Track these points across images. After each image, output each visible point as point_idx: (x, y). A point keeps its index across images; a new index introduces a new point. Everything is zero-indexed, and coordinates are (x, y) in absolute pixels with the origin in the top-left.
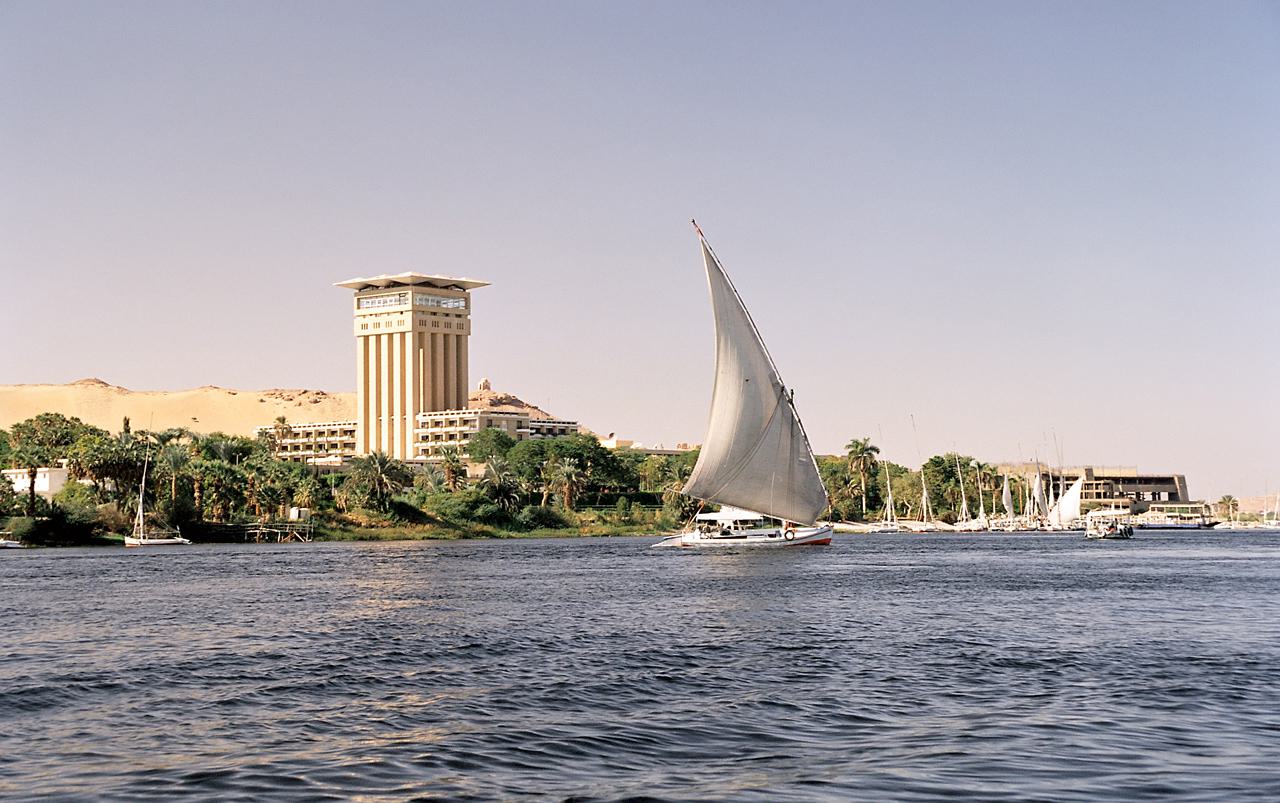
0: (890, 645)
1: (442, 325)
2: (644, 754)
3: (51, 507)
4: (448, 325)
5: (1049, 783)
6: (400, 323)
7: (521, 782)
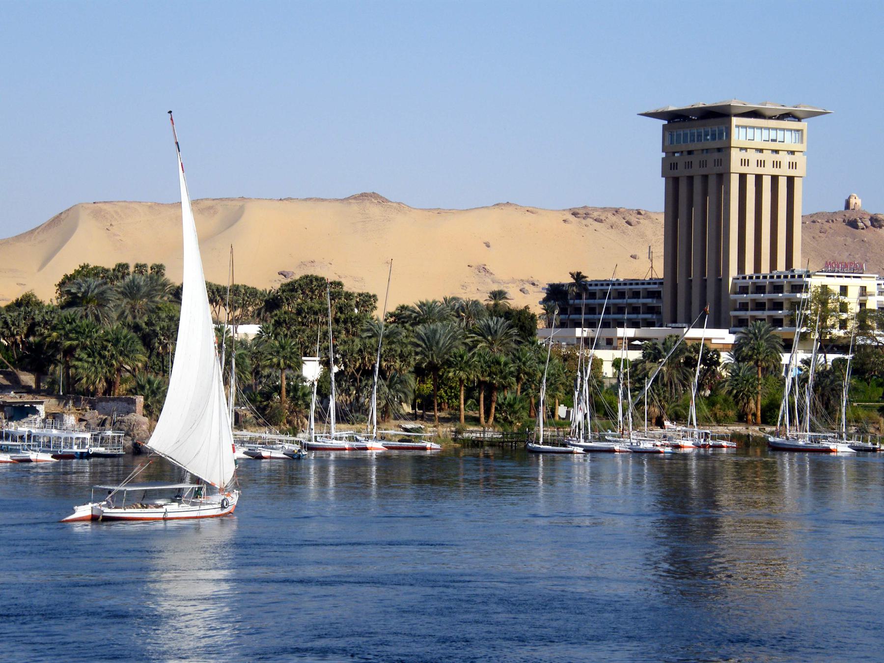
1: (769, 164)
4: (703, 164)
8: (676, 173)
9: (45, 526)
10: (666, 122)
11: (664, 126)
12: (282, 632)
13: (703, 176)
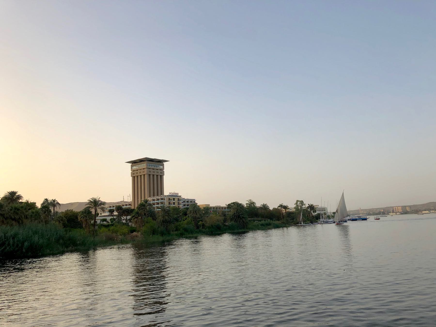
0: (39, 261)
1: (156, 172)
2: (86, 285)
3: (180, 210)
4: (154, 172)
5: (317, 315)
6: (144, 172)
7: (348, 314)
8: (134, 175)
9: (113, 320)
10: (132, 164)
11: (131, 165)
12: (29, 228)
13: (137, 176)
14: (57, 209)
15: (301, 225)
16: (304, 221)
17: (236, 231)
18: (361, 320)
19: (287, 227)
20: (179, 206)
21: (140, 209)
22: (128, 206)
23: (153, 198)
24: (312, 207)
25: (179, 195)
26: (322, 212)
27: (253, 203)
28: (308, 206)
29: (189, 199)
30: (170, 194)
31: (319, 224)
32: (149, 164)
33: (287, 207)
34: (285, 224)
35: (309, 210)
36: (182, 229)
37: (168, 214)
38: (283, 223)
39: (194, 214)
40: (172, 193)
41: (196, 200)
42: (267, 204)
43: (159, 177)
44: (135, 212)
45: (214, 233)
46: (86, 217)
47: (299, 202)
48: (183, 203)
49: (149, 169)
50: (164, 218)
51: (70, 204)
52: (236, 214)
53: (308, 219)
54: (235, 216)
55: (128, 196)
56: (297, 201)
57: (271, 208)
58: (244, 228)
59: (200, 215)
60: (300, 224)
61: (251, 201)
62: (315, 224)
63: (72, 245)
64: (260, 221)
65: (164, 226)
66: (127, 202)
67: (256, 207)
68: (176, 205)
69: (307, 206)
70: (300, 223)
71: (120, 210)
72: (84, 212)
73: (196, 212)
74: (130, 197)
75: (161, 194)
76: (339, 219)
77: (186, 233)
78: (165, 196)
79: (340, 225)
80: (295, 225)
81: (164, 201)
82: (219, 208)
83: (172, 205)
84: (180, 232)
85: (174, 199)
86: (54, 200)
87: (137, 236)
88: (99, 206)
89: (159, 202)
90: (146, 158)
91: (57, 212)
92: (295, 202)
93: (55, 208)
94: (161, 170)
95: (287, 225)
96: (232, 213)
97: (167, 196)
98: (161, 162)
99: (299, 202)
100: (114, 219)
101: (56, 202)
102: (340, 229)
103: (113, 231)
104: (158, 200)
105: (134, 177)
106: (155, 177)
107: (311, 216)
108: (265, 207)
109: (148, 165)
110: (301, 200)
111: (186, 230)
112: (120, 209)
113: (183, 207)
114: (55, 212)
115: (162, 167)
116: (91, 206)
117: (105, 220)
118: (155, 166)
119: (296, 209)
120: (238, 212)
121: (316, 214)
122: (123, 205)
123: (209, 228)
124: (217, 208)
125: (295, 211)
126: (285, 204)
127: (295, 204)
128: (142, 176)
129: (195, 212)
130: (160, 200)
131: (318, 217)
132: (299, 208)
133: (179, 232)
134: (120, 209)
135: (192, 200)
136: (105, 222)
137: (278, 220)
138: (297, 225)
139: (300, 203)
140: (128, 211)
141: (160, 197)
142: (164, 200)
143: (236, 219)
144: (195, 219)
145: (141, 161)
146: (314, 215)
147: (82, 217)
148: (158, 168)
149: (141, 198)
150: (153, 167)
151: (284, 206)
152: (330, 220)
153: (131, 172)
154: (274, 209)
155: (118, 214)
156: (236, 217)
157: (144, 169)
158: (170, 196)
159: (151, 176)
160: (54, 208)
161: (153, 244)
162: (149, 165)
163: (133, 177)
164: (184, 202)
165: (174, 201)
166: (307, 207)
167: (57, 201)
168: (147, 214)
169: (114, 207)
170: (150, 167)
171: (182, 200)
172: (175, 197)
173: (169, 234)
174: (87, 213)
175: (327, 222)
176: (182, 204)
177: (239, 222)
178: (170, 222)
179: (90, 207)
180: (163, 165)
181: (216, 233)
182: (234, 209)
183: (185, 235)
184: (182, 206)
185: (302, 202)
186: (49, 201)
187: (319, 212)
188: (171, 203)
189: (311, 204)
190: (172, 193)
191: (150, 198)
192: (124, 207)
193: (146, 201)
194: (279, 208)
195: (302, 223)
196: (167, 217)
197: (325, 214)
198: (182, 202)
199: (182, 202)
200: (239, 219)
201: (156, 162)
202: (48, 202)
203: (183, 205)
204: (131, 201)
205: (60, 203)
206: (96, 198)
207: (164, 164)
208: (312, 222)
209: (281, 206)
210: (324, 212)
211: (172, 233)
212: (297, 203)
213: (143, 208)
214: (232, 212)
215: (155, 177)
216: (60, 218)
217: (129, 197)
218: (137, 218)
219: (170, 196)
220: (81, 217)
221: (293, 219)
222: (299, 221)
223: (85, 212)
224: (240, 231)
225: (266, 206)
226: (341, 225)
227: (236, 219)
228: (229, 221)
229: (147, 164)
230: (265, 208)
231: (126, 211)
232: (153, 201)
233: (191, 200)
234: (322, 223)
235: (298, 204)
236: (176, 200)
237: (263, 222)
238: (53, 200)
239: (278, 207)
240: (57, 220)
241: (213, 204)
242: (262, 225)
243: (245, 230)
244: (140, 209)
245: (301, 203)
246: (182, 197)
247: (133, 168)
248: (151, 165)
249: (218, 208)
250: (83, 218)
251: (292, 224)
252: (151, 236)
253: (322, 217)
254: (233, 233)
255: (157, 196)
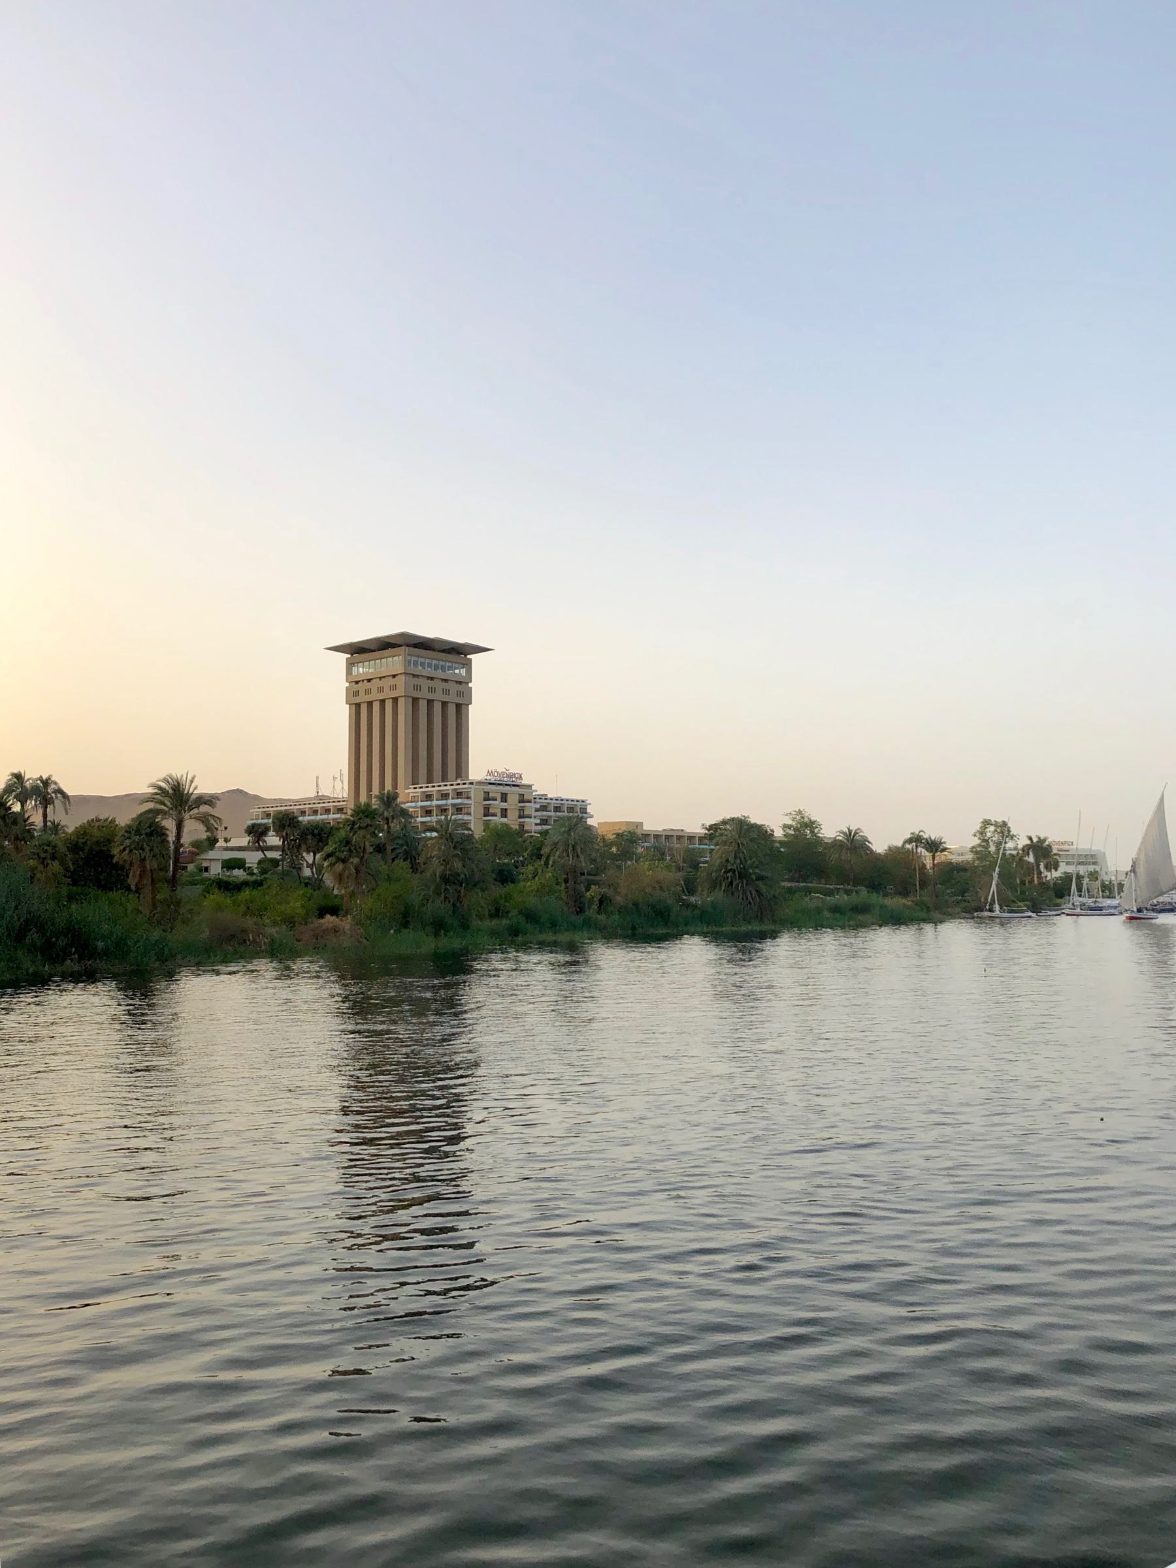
6: (393, 688)
8: (358, 700)
10: (349, 656)
14: (56, 814)
15: (991, 917)
16: (1007, 903)
17: (727, 929)
18: (23, 1405)
19: (937, 922)
20: (522, 825)
21: (357, 826)
22: (331, 816)
23: (427, 787)
24: (1041, 849)
25: (524, 782)
26: (1082, 870)
27: (811, 825)
28: (1029, 842)
29: (562, 800)
30: (489, 777)
31: (1064, 913)
32: (414, 658)
33: (941, 843)
34: (928, 909)
35: (1031, 859)
36: (514, 912)
37: (464, 851)
38: (921, 905)
39: (568, 856)
40: (496, 774)
41: (590, 804)
42: (862, 832)
43: (452, 710)
44: (337, 840)
45: (640, 931)
46: (142, 849)
47: (992, 828)
48: (539, 813)
49: (414, 676)
50: (448, 867)
51: (131, 797)
52: (733, 865)
53: (1023, 892)
54: (731, 870)
55: (334, 778)
56: (986, 823)
57: (879, 846)
58: (761, 920)
59: (593, 861)
60: (987, 914)
61: (803, 818)
62: (1050, 913)
63: (75, 953)
64: (830, 893)
65: (446, 898)
66: (330, 798)
67: (821, 839)
68: (512, 821)
69: (1023, 842)
70: (987, 907)
71: (288, 830)
72: (135, 829)
73: (573, 847)
74: (342, 782)
75: (458, 776)
76: (1139, 900)
77: (529, 926)
78: (471, 783)
79: (1143, 921)
80: (967, 915)
81: (466, 801)
82: (679, 838)
83: (498, 819)
84: (508, 922)
85: (504, 798)
86: (47, 780)
87: (335, 931)
88: (190, 809)
89: (446, 805)
90: (403, 635)
91: (56, 827)
92: (978, 827)
93: (50, 809)
94: (460, 683)
95: (936, 915)
96: (718, 861)
97: (480, 783)
98: (459, 652)
99: (992, 828)
100: (275, 862)
101: (53, 786)
102: (1143, 939)
103: (248, 908)
104: (445, 796)
105: (358, 706)
106: (437, 708)
107: (1036, 882)
108: (854, 844)
109: (410, 662)
110: (1000, 820)
111: (531, 917)
112: (289, 825)
113: (539, 828)
114: (49, 824)
115: (463, 672)
116: (163, 807)
117: (239, 864)
118: (436, 667)
119: (977, 853)
120: (741, 855)
121: (1056, 874)
122: (303, 813)
123: (621, 910)
124: (668, 837)
125: (974, 861)
126: (931, 834)
127: (975, 836)
128: (374, 703)
129: (570, 849)
130: (452, 799)
131: (1061, 890)
132: (992, 849)
133: (505, 921)
134: (289, 825)
135: (549, 801)
136: (236, 872)
137: (905, 893)
138: (975, 914)
139: (996, 831)
140: (319, 834)
141: (453, 787)
142: (468, 798)
143: (731, 884)
144: (572, 876)
145: (385, 645)
146: (1049, 878)
147: (124, 850)
148: (448, 674)
149: (370, 789)
150: (428, 672)
151: (926, 839)
152: (1109, 902)
153: (347, 684)
154: (893, 852)
155: (281, 843)
156: (734, 873)
157: (394, 676)
158: (490, 784)
159: (423, 705)
160: (46, 808)
161: (405, 965)
162: (416, 664)
163: (354, 706)
164: (544, 808)
165: (504, 805)
166: (1024, 847)
167: (55, 783)
168: (389, 848)
169: (268, 815)
170: (419, 670)
171: (535, 802)
172: (508, 788)
173: (465, 926)
174: (143, 832)
175: (1096, 910)
176: (535, 817)
177: (744, 892)
178: (472, 884)
179: (157, 812)
180: (468, 665)
181: (651, 931)
182: (725, 843)
183: (528, 934)
184: (536, 824)
185: (1004, 829)
186: (28, 784)
187: (1070, 869)
188: (491, 811)
189: (1039, 838)
190: (496, 774)
191: (415, 788)
192: (307, 818)
193: (389, 800)
194: (908, 846)
195: (997, 907)
196: (457, 865)
197: (1094, 876)
198: (537, 810)
199: (537, 810)
200: (745, 882)
201: (443, 651)
202: (23, 787)
203: (538, 821)
204: (345, 795)
205: (70, 792)
206: (182, 776)
207: (470, 660)
208: (1036, 908)
209: (917, 839)
210: (1091, 868)
211: (475, 923)
212: (982, 832)
213: (368, 825)
214: (713, 855)
215: (437, 708)
216: (46, 847)
217: (338, 781)
218: (344, 861)
219: (490, 784)
220: (122, 847)
221: (963, 892)
222: (986, 899)
223: (138, 832)
224: (744, 928)
225: (857, 837)
226: (1150, 921)
227: (731, 884)
228: (703, 890)
229: (409, 658)
230: (853, 844)
231: (313, 835)
232: (427, 801)
233: (570, 802)
234: (1078, 911)
235: (989, 835)
236: (513, 799)
237: (841, 898)
238: (41, 779)
239: (905, 842)
240: (34, 853)
241: (652, 825)
242: (836, 909)
243: (764, 927)
244: (357, 826)
245: (1002, 832)
246: (536, 791)
247: (354, 669)
248: (422, 664)
249: (673, 836)
250: (131, 851)
251: (958, 910)
252: (392, 931)
253: (1079, 890)
254: (716, 937)
255: (443, 781)
